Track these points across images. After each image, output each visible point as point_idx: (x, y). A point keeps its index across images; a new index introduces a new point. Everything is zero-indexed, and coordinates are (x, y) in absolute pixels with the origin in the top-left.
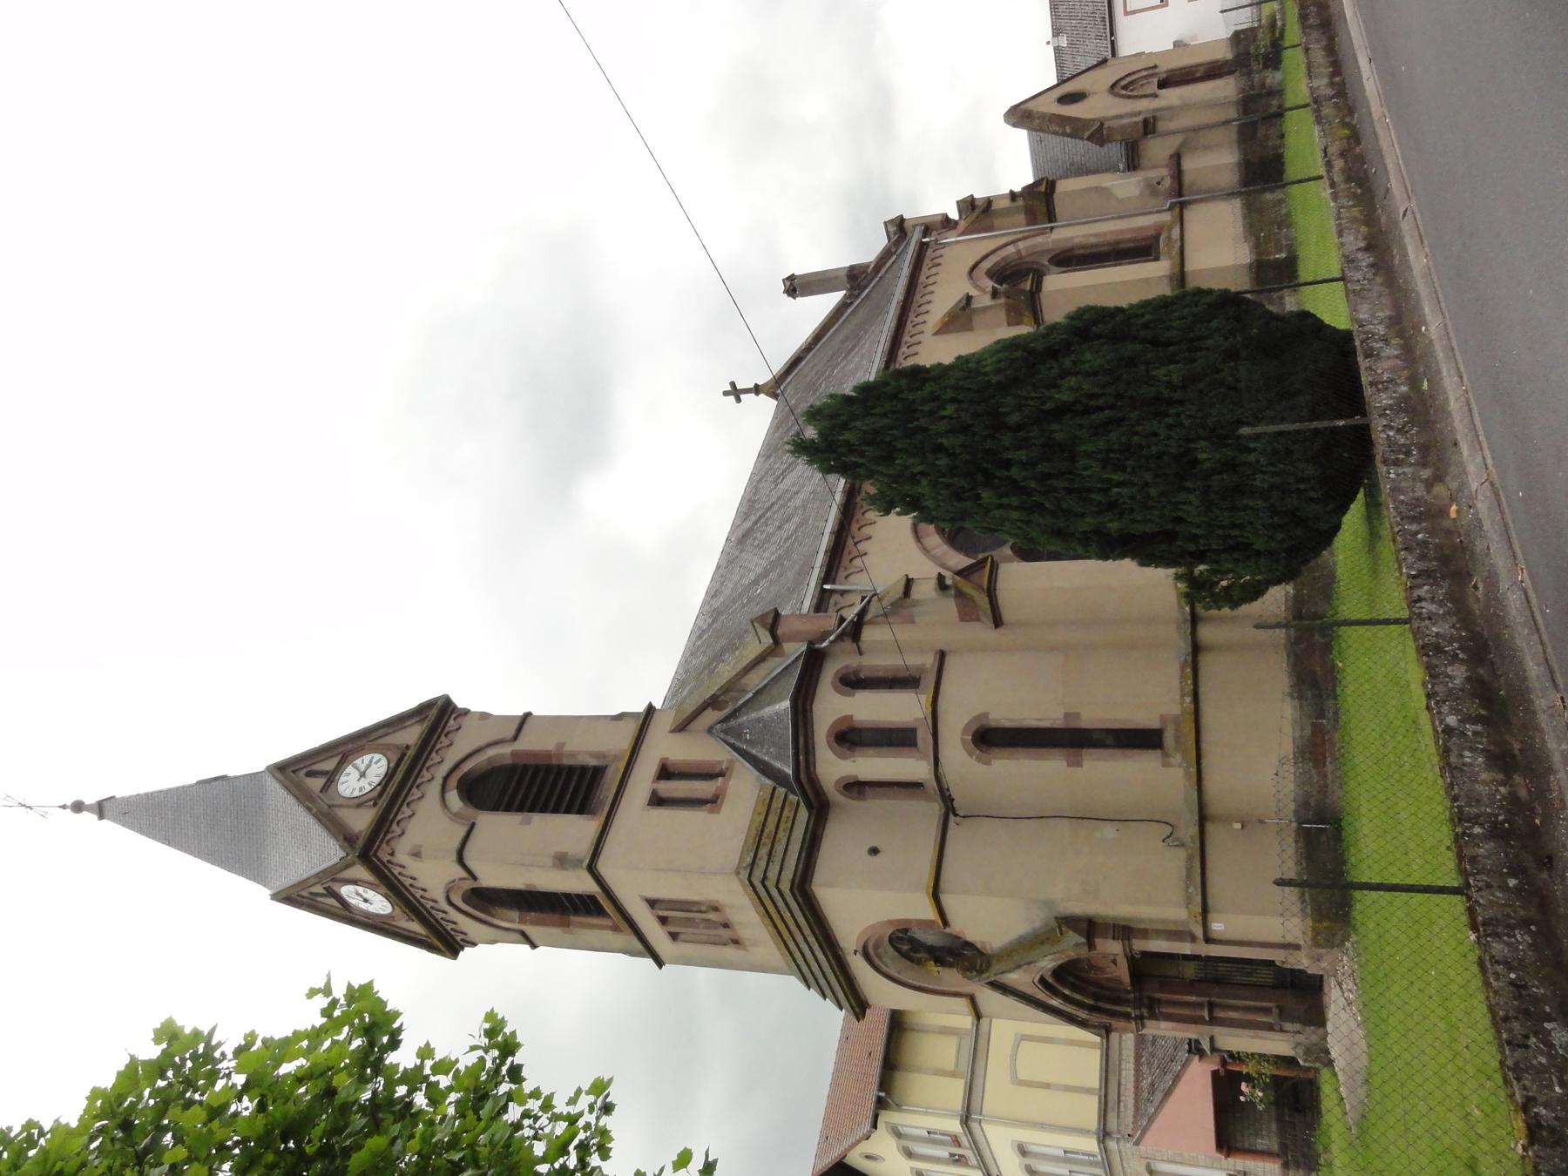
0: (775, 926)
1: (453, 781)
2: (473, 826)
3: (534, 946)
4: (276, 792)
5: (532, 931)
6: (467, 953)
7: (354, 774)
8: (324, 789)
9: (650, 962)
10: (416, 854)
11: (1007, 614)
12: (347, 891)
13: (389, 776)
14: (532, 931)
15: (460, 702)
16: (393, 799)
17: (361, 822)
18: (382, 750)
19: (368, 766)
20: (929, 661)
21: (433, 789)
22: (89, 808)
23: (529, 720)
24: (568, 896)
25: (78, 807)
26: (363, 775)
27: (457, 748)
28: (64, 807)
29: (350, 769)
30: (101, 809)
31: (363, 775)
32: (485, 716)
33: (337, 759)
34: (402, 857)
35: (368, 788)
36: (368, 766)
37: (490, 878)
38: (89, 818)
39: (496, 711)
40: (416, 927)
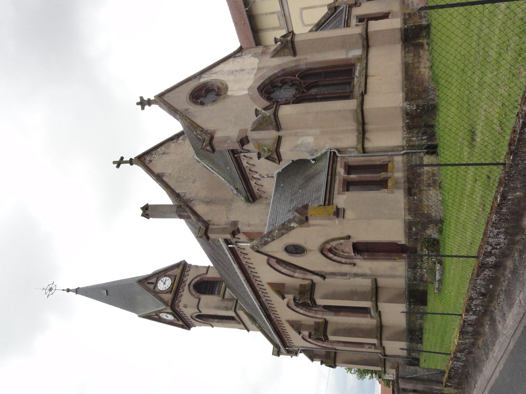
0: (378, 152)
1: (192, 287)
2: (200, 299)
3: (248, 331)
4: (139, 288)
5: (212, 323)
6: (193, 329)
7: (162, 283)
8: (154, 288)
9: (246, 331)
10: (185, 306)
11: (346, 216)
12: (161, 315)
13: (172, 284)
14: (212, 323)
15: (189, 262)
16: (176, 291)
17: (168, 297)
18: (169, 276)
19: (166, 281)
20: (341, 200)
21: (186, 288)
22: (72, 291)
23: (210, 269)
24: (222, 316)
25: (68, 290)
26: (164, 283)
27: (190, 277)
28: (64, 290)
29: (160, 282)
30: (77, 291)
31: (164, 283)
32: (197, 267)
33: (156, 278)
34: (181, 307)
35: (167, 288)
36: (166, 281)
37: (205, 312)
38: (65, 292)
39: (199, 264)
40: (181, 323)
